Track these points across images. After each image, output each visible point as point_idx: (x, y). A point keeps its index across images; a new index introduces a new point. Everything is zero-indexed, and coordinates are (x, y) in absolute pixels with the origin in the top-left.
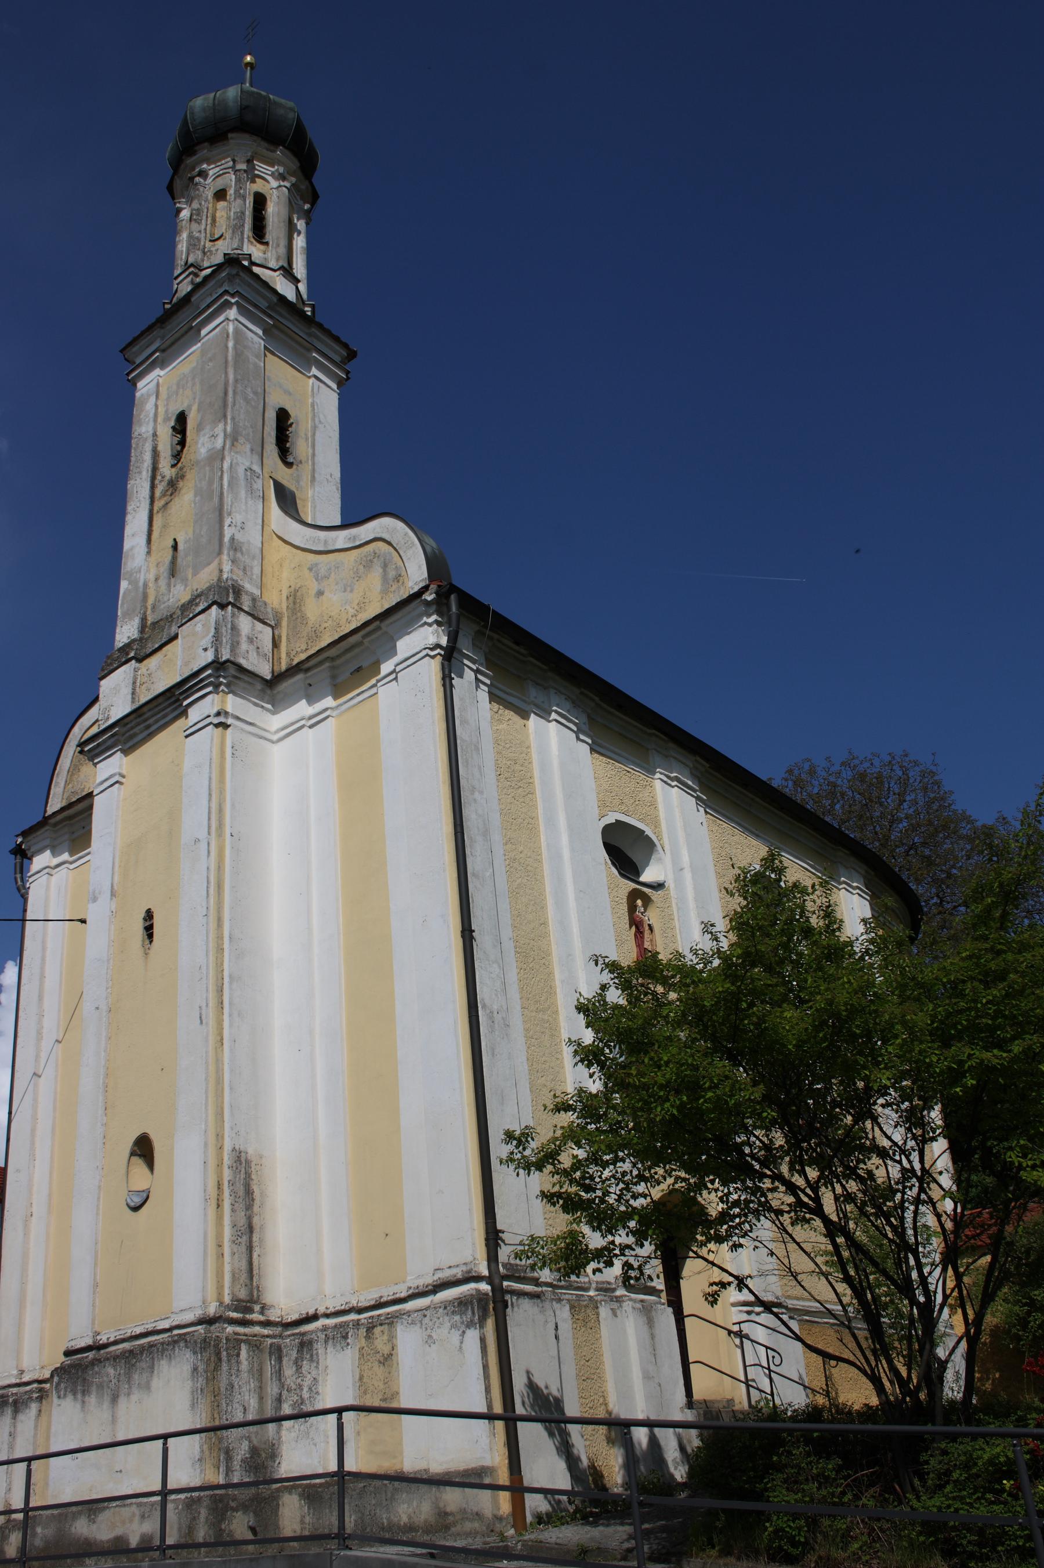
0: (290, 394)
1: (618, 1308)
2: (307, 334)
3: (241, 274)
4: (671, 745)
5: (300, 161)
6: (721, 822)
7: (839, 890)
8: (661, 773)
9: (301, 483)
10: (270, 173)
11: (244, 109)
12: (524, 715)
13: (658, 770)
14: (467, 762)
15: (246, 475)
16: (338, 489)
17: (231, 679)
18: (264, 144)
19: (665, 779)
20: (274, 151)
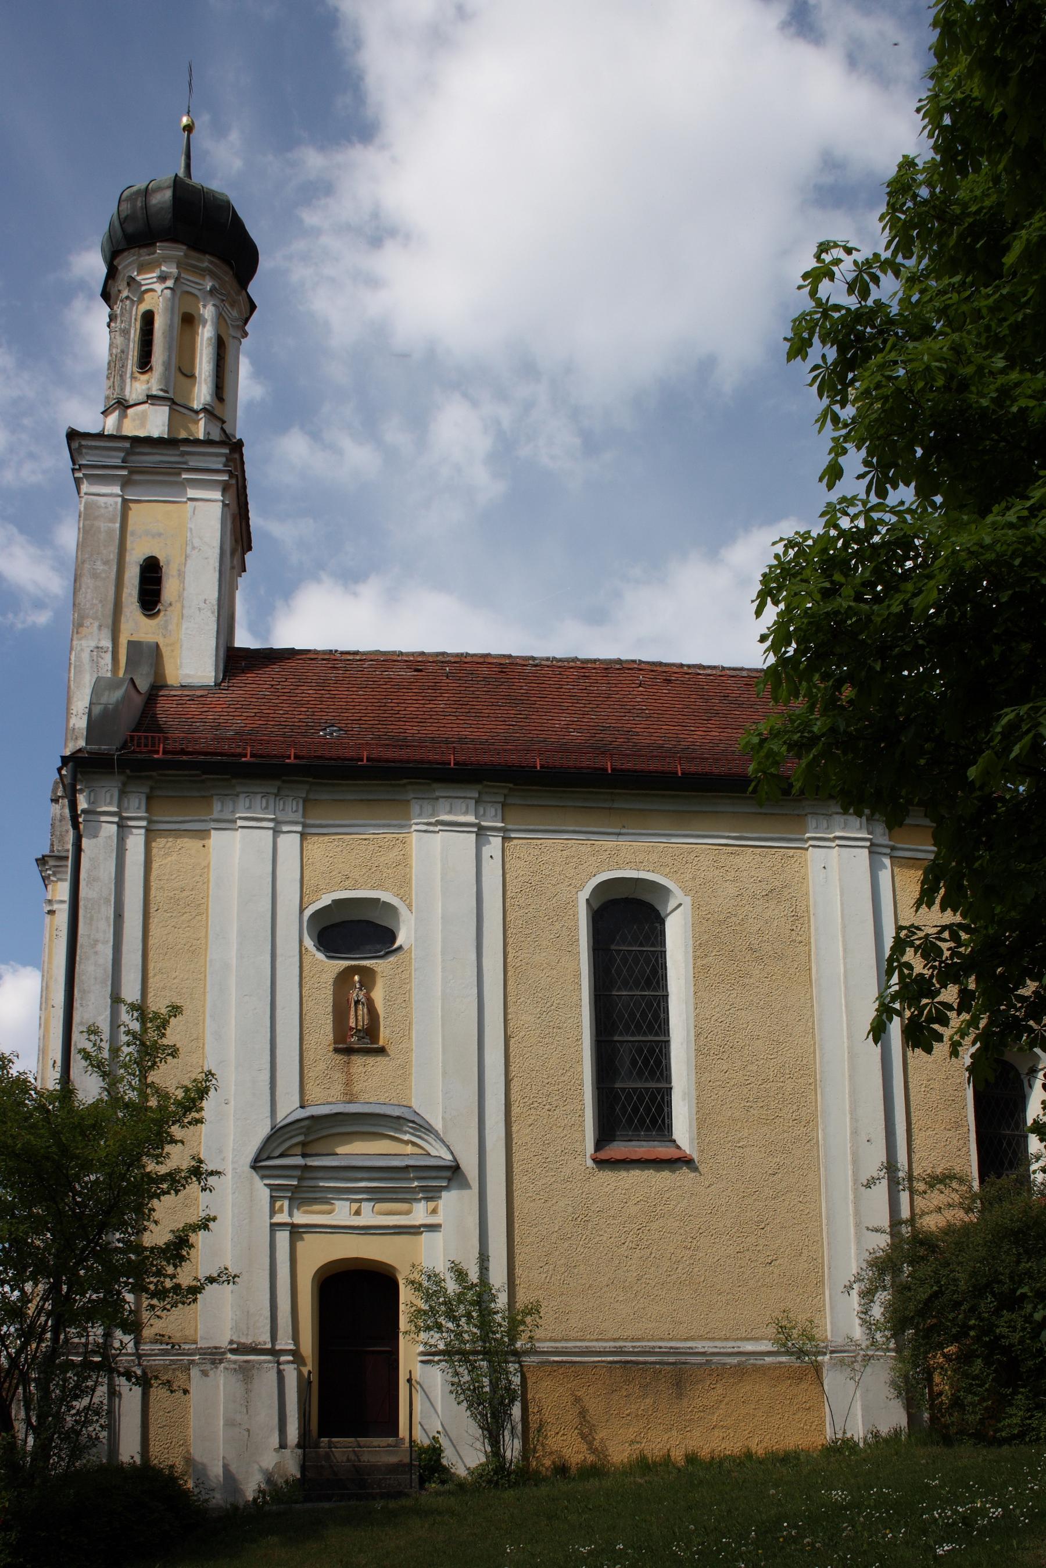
0: (160, 535)
1: (212, 1369)
2: (179, 455)
3: (84, 443)
4: (435, 785)
5: (183, 243)
6: (539, 842)
7: (807, 849)
8: (417, 824)
9: (170, 627)
10: (155, 280)
11: (124, 222)
12: (203, 834)
13: (413, 821)
14: (91, 919)
15: (91, 656)
16: (213, 613)
17: (53, 869)
18: (144, 251)
19: (424, 828)
20: (155, 252)
